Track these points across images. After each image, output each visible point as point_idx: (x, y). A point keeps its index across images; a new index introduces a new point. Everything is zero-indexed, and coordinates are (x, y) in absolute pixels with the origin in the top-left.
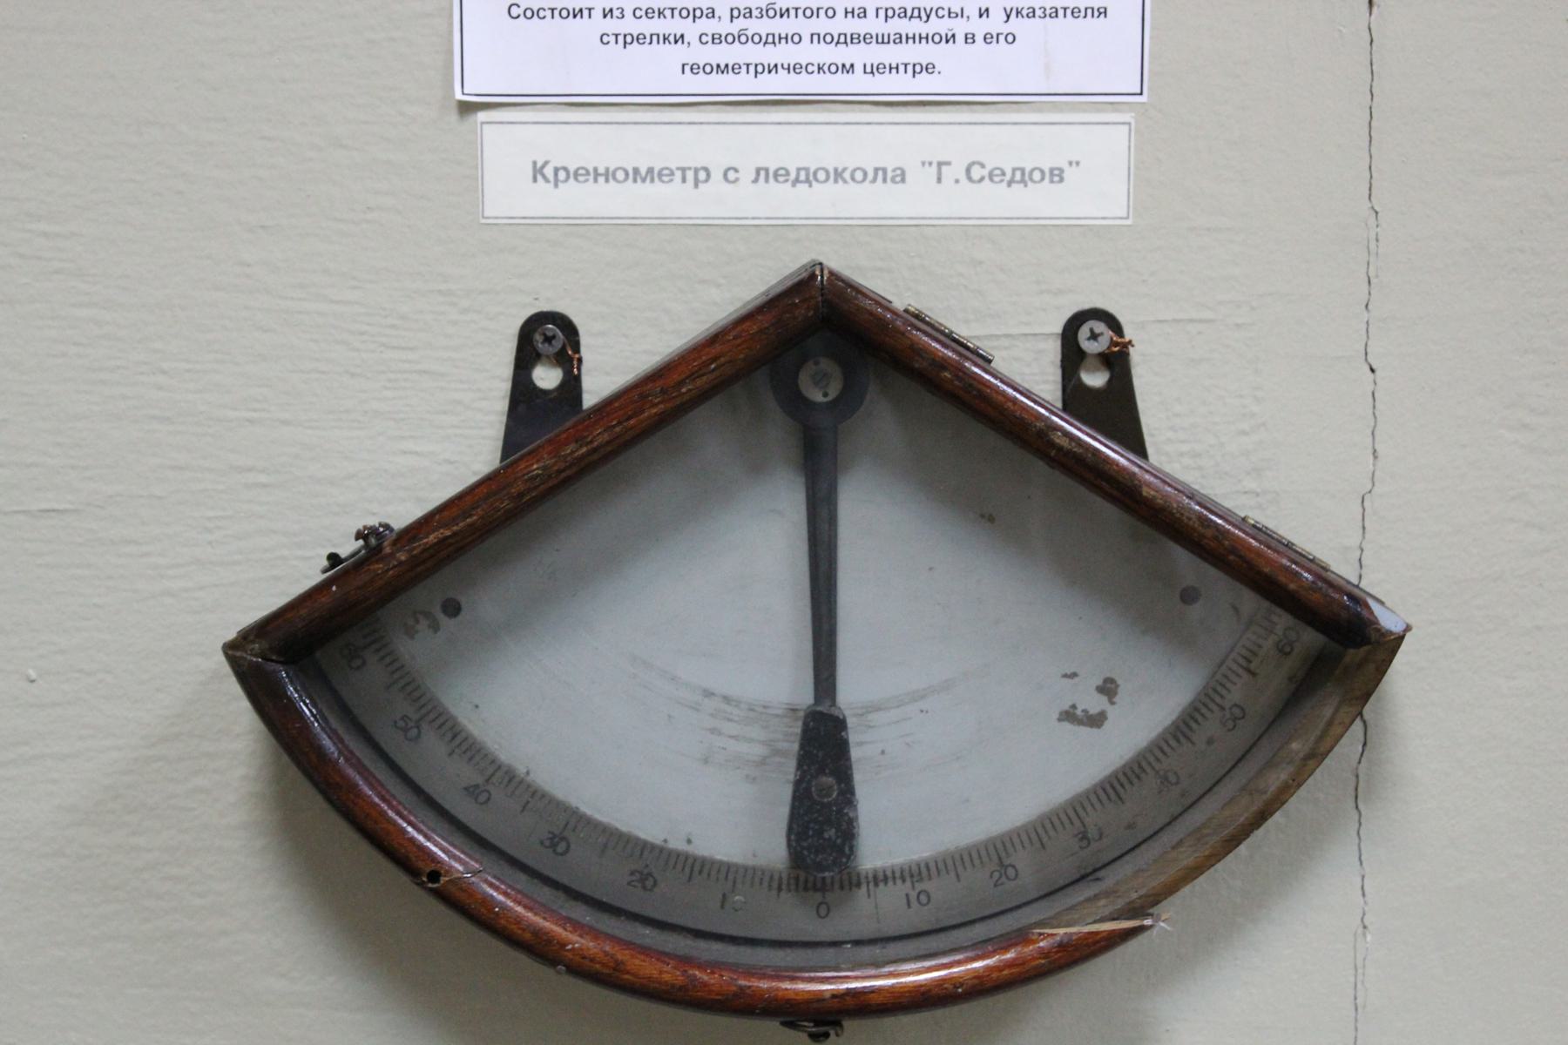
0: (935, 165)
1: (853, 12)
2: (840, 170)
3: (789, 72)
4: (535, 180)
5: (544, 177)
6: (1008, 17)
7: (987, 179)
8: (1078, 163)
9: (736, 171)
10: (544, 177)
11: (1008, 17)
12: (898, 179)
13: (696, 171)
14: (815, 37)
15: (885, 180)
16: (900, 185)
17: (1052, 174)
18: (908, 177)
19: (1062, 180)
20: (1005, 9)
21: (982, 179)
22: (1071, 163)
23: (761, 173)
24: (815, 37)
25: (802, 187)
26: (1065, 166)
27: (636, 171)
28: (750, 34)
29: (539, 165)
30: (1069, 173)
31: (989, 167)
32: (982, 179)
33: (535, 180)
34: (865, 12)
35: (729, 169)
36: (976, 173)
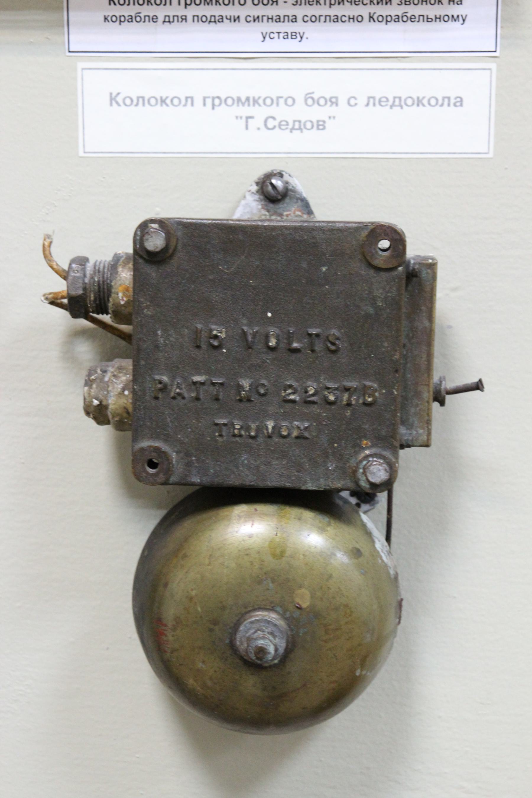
0: (244, 119)
1: (272, 19)
2: (421, 98)
3: (427, 16)
4: (111, 105)
5: (117, 103)
6: (264, 38)
7: (277, 128)
8: (334, 117)
9: (355, 98)
10: (117, 103)
11: (264, 38)
12: (458, 104)
13: (213, 99)
14: (196, 18)
15: (449, 105)
16: (460, 108)
17: (318, 125)
18: (464, 103)
19: (324, 128)
20: (262, 33)
21: (274, 127)
22: (330, 118)
23: (371, 101)
24: (196, 18)
25: (397, 109)
26: (326, 119)
27: (239, 99)
28: (409, 15)
29: (114, 95)
30: (329, 124)
31: (279, 119)
32: (274, 127)
33: (111, 105)
34: (296, 19)
35: (293, 105)
36: (271, 123)
